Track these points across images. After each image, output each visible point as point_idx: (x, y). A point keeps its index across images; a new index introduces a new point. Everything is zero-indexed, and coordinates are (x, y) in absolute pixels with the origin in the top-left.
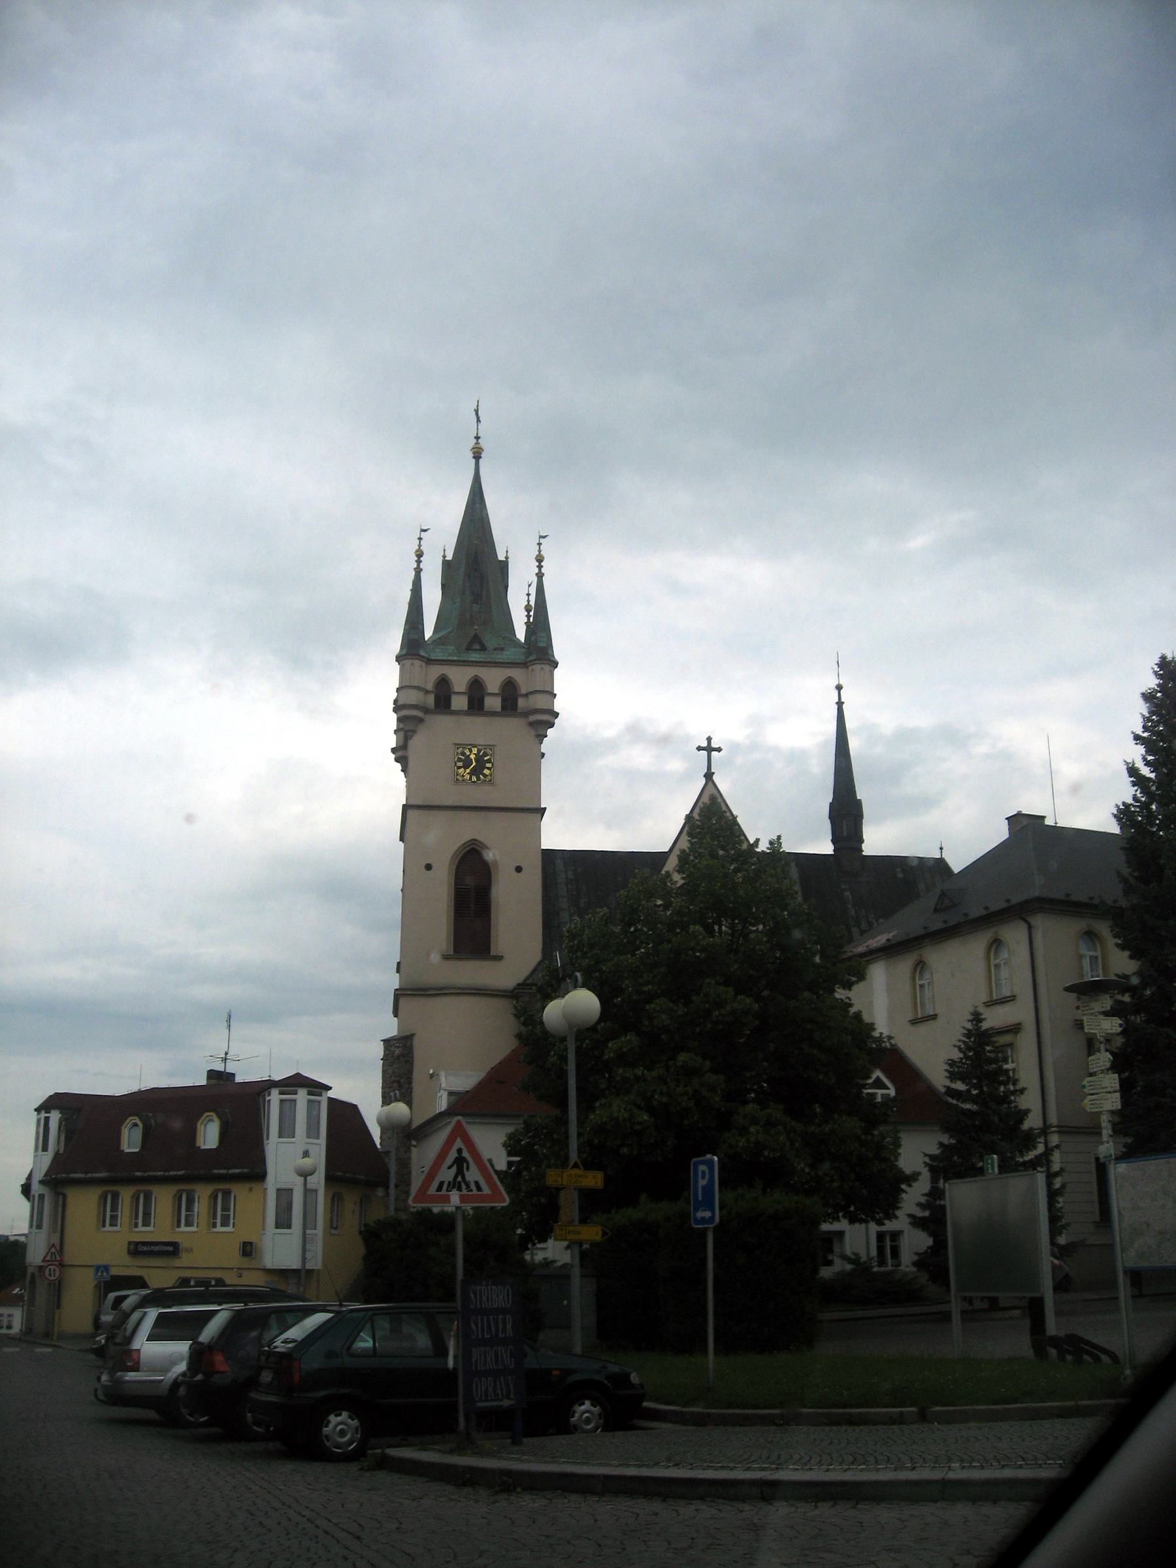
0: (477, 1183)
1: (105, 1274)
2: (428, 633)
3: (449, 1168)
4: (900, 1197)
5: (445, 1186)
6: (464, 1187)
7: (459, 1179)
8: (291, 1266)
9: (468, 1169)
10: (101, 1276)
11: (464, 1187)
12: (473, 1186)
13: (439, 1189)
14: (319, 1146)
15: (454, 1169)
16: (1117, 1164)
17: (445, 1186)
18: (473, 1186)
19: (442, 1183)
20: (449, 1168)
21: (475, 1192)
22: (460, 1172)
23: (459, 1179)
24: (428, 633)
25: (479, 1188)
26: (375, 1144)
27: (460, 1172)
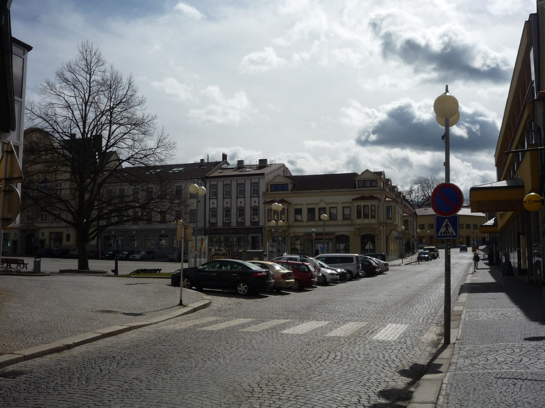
0: (452, 232)
1: (451, 229)
2: (286, 331)
3: (444, 227)
4: (426, 124)
5: (443, 233)
6: (448, 233)
7: (447, 231)
8: (296, 294)
9: (449, 228)
10: (445, 233)
11: (448, 233)
12: (451, 233)
13: (441, 234)
14: (344, 208)
15: (445, 227)
16: (176, 228)
17: (443, 233)
18: (451, 233)
19: (442, 232)
20: (444, 227)
21: (451, 235)
22: (447, 229)
23: (447, 231)
24: (286, 331)
25: (452, 234)
26: (20, 168)
27: (447, 229)
